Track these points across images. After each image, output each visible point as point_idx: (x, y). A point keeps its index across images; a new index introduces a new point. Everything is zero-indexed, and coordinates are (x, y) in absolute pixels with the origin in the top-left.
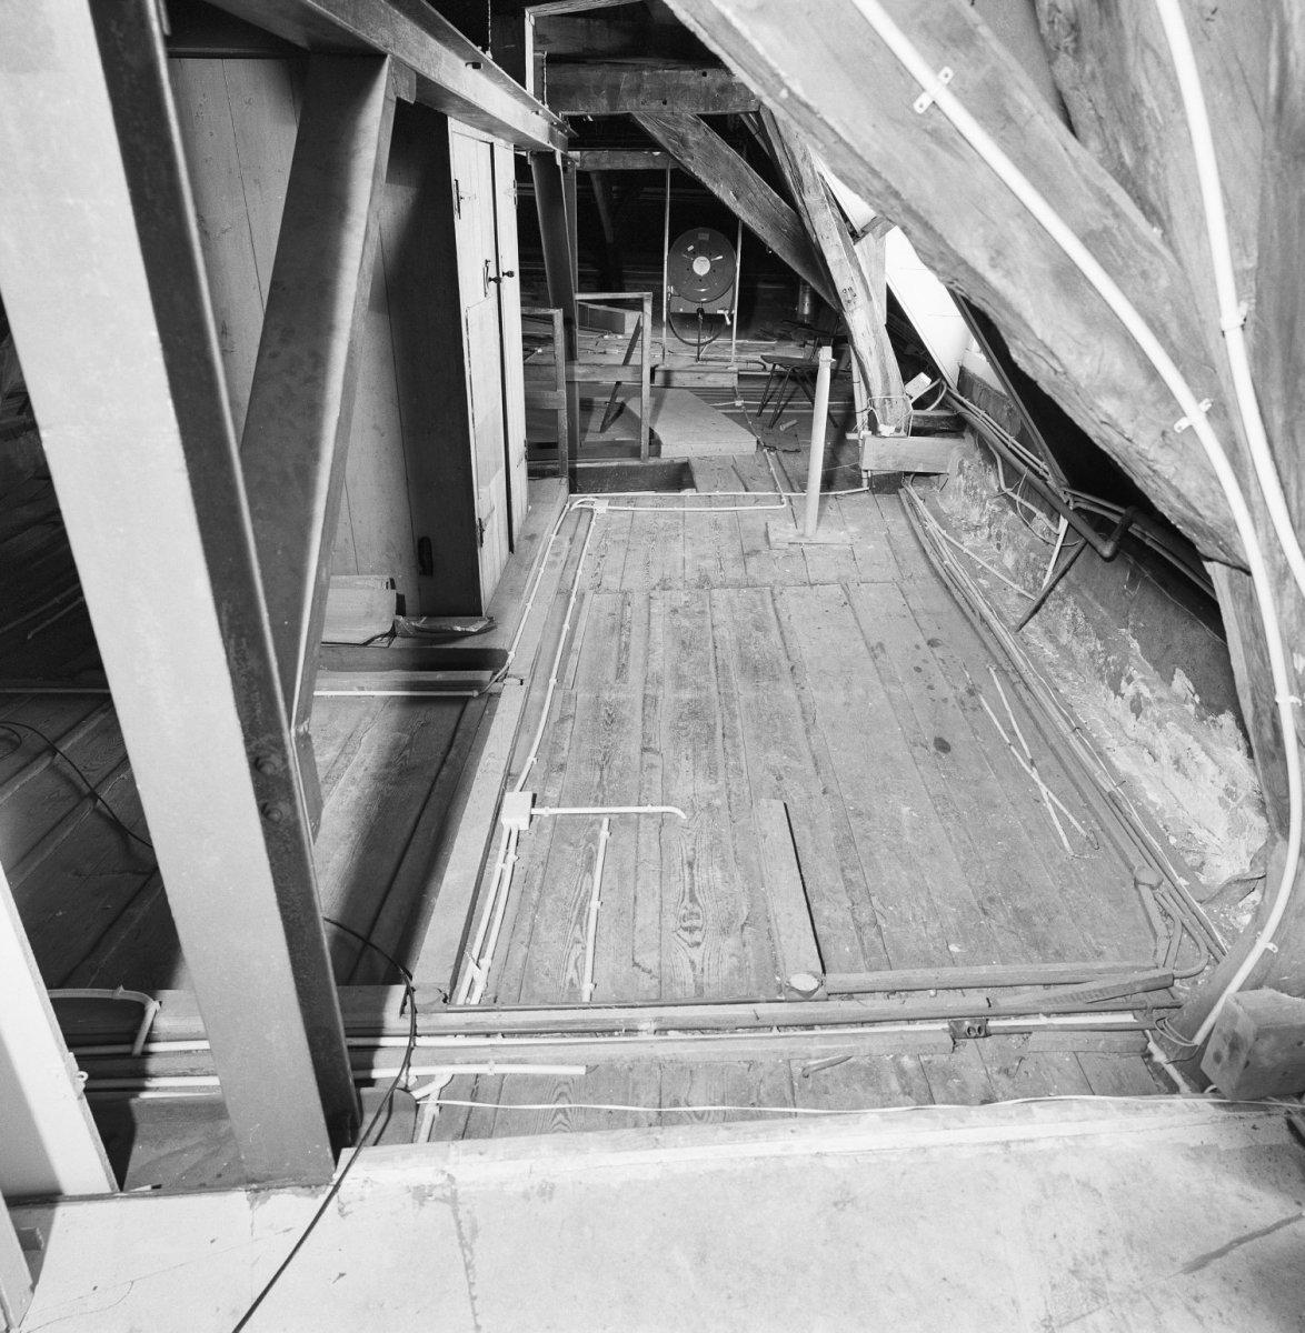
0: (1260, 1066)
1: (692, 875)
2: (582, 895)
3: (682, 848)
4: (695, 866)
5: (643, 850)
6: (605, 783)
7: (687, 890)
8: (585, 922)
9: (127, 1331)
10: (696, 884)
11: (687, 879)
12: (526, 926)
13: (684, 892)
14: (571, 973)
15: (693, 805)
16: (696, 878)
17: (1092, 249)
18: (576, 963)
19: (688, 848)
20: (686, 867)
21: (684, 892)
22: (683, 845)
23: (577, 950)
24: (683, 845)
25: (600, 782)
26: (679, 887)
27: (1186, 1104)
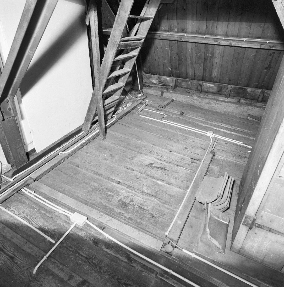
0: (166, 16)
1: (7, 255)
2: (33, 222)
3: (20, 260)
4: (9, 259)
5: (31, 245)
6: (77, 255)
7: (4, 249)
8: (23, 219)
9: (283, 246)
10: (3, 254)
11: (8, 253)
12: (35, 206)
13: (5, 248)
14: (12, 209)
15: (37, 280)
16: (5, 255)
17: (38, 270)
18: (14, 211)
19: (19, 262)
20: (13, 256)
21: (5, 248)
22: (22, 261)
23: (17, 213)
24: (22, 261)
25: (79, 253)
26: (8, 248)
27: (175, 9)
